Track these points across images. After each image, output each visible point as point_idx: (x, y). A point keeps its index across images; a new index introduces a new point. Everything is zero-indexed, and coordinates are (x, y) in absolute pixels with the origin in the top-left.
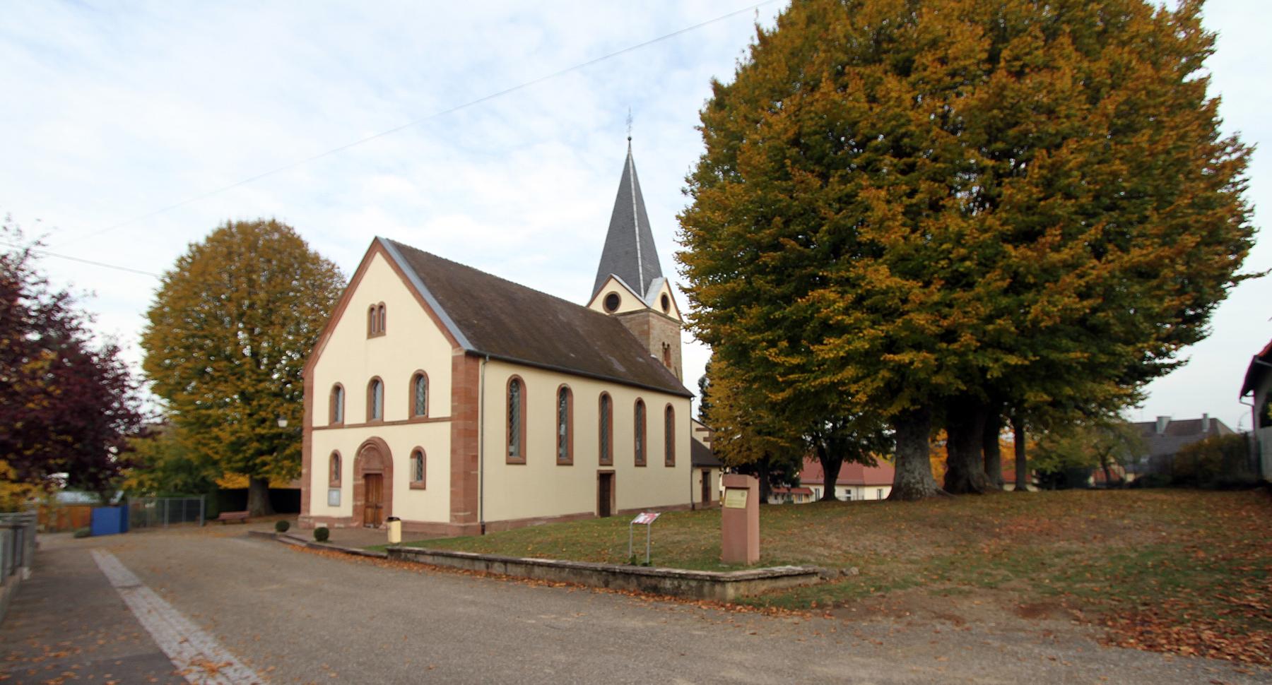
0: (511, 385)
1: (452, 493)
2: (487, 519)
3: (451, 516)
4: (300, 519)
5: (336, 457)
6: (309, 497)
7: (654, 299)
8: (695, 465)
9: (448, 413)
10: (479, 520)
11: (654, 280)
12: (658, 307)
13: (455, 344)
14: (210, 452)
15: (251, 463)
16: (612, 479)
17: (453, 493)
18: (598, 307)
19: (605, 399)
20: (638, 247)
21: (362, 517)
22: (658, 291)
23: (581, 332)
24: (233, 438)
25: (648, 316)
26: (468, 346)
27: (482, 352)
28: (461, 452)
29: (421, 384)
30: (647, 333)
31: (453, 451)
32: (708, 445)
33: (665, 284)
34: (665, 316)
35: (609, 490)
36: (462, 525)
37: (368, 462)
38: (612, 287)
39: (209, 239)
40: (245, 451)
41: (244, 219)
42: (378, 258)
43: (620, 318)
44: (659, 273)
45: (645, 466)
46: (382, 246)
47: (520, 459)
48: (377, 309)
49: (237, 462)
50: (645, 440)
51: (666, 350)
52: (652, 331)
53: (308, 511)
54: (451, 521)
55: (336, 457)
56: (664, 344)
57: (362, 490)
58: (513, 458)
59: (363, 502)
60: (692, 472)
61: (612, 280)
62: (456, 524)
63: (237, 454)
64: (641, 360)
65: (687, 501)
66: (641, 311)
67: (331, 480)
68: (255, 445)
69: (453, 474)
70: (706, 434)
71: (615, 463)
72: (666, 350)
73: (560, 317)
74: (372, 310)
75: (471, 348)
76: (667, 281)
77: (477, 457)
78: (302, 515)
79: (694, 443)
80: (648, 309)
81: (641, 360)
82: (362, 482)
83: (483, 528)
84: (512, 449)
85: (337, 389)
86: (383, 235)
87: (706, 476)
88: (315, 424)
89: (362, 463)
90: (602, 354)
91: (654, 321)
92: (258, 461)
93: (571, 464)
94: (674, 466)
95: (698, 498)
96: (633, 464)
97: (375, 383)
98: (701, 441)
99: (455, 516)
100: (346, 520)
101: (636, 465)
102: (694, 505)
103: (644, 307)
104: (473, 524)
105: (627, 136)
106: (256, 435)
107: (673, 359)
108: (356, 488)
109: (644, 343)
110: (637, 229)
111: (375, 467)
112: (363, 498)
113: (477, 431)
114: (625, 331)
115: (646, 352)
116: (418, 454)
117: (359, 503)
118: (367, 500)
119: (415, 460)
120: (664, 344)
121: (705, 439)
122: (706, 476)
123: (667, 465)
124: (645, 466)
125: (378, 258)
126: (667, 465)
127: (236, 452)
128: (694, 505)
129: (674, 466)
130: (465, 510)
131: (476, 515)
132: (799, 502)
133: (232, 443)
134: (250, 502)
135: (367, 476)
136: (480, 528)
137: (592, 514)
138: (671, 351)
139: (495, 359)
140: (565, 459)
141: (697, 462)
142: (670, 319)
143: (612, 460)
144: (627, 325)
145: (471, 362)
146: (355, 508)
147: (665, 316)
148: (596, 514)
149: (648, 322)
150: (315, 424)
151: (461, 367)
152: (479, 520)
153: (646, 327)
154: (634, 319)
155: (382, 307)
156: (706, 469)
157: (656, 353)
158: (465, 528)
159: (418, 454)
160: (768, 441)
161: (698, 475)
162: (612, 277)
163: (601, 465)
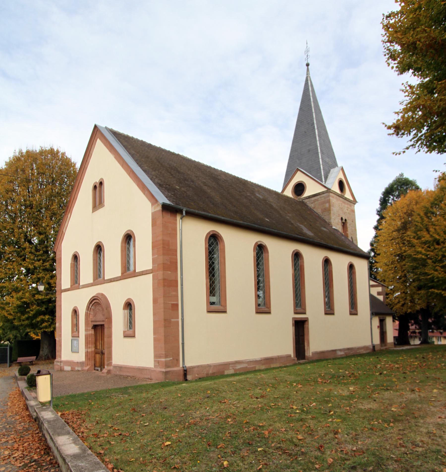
0: (210, 239)
1: (155, 340)
2: (188, 364)
3: (155, 361)
4: (55, 363)
5: (75, 312)
6: (61, 346)
7: (333, 183)
8: (374, 313)
9: (150, 267)
10: (181, 365)
11: (332, 170)
12: (336, 189)
13: (152, 199)
14: (6, 314)
15: (34, 321)
16: (306, 326)
17: (156, 340)
18: (289, 193)
19: (297, 256)
20: (318, 145)
21: (93, 362)
22: (336, 176)
23: (275, 206)
24: (19, 303)
25: (329, 196)
26: (163, 199)
27: (181, 207)
28: (161, 301)
29: (132, 243)
30: (328, 210)
31: (155, 301)
32: (381, 298)
33: (341, 172)
34: (342, 197)
35: (303, 335)
36: (164, 370)
37: (95, 315)
38: (299, 177)
39: (7, 164)
40: (29, 312)
41: (30, 149)
42: (99, 144)
43: (306, 201)
44: (335, 165)
45: (333, 314)
46: (102, 135)
47: (221, 308)
48: (98, 186)
49: (24, 321)
50: (333, 292)
51: (344, 224)
52: (332, 208)
53: (60, 357)
54: (155, 366)
55: (75, 312)
56: (342, 219)
57: (92, 339)
58: (213, 307)
59: (93, 349)
60: (371, 319)
61: (299, 172)
62: (159, 369)
63: (24, 315)
64: (325, 229)
65: (368, 343)
66: (323, 193)
67: (73, 332)
68: (35, 307)
69: (155, 322)
70: (380, 289)
71: (307, 312)
72: (344, 224)
73: (257, 195)
74: (95, 187)
75: (167, 202)
76: (342, 169)
77: (177, 305)
78: (56, 360)
79: (372, 298)
80: (329, 190)
81: (325, 229)
82: (92, 332)
83: (185, 372)
84: (213, 299)
85: (76, 258)
86: (102, 124)
87: (382, 322)
88: (63, 288)
89: (91, 317)
90: (292, 222)
91: (334, 200)
92: (39, 319)
93: (269, 313)
94: (356, 314)
95: (377, 341)
96: (324, 313)
97: (99, 248)
98: (375, 294)
99: (158, 362)
100: (81, 364)
101: (326, 314)
102: (374, 347)
103: (325, 189)
104: (175, 369)
105: (306, 62)
106: (36, 300)
107: (349, 231)
108: (87, 337)
109: (326, 218)
110: (316, 131)
111: (100, 319)
112: (93, 346)
113: (177, 281)
114: (310, 210)
115: (328, 224)
116: (129, 305)
117: (90, 350)
118: (96, 347)
119: (127, 311)
120: (342, 219)
121: (379, 294)
122: (382, 322)
123: (351, 314)
124: (333, 314)
125: (99, 144)
126: (351, 314)
127: (23, 313)
128: (374, 347)
129: (356, 314)
130: (166, 356)
131: (178, 360)
132: (439, 343)
133: (19, 307)
134: (41, 349)
135: (95, 327)
136: (182, 373)
137: (290, 356)
138: (348, 225)
139: (191, 214)
140: (263, 308)
141: (374, 311)
142: (346, 199)
143: (305, 309)
144: (311, 206)
145: (168, 217)
146: (87, 354)
147: (342, 197)
148: (292, 356)
149: (329, 201)
150: (63, 288)
151: (159, 221)
152: (181, 365)
153: (327, 205)
154: (317, 200)
155: (101, 183)
156: (382, 317)
157: (337, 225)
158: (166, 373)
159: (129, 305)
160: (433, 293)
161: (376, 321)
162: (298, 170)
163: (296, 313)
